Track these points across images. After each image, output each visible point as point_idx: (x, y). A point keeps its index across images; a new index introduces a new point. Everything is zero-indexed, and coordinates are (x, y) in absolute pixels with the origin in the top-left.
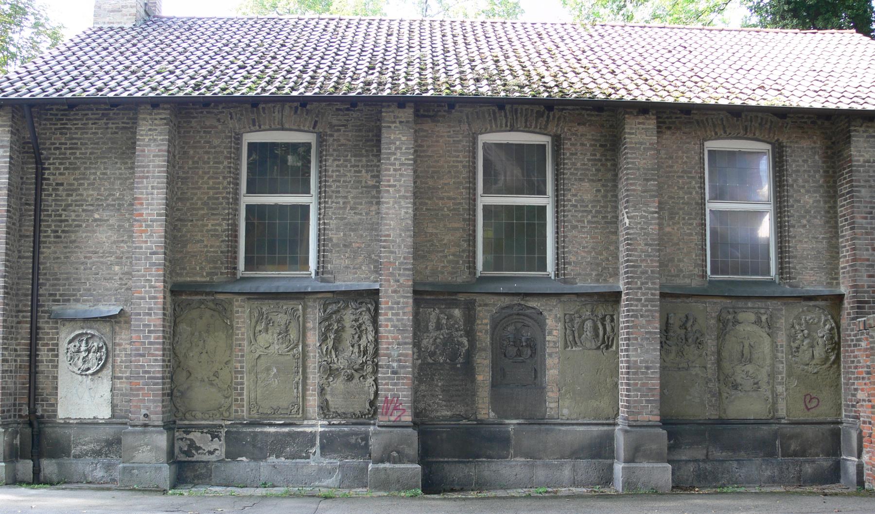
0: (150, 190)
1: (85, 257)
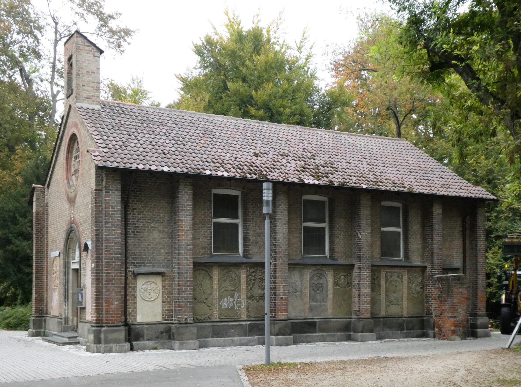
0: (185, 216)
1: (148, 245)
